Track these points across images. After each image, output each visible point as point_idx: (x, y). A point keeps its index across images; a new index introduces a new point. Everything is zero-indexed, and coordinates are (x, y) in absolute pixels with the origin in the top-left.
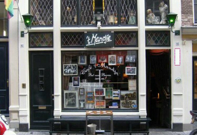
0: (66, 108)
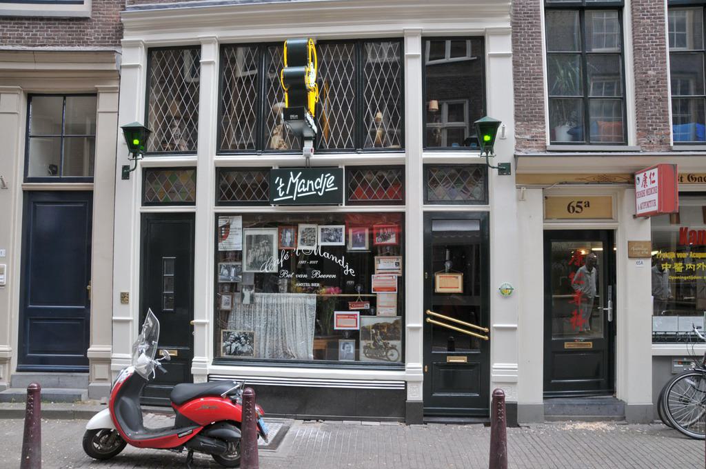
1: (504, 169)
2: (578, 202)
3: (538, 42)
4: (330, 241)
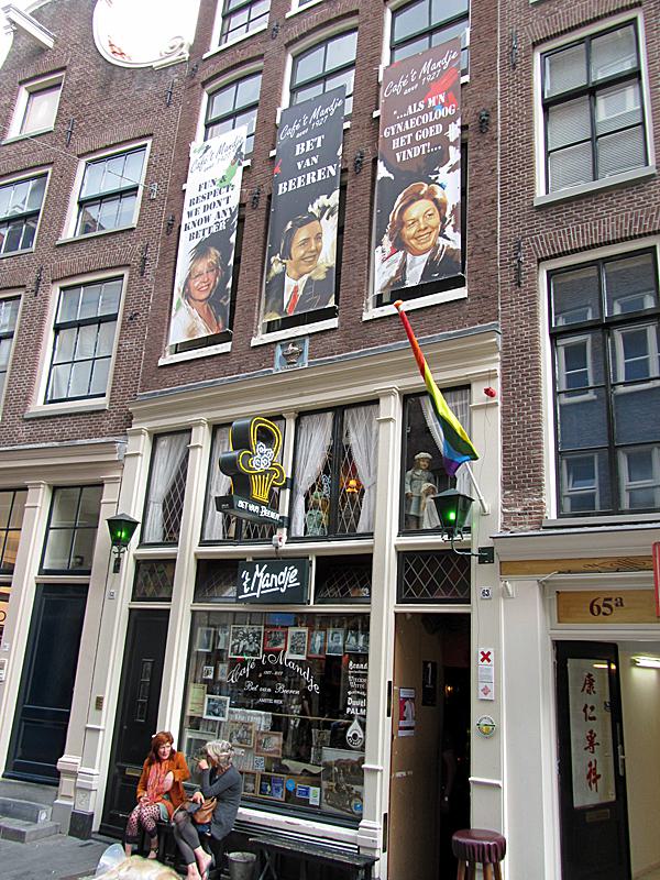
0: (378, 796)
1: (487, 555)
2: (606, 600)
3: (535, 382)
4: (215, 715)
